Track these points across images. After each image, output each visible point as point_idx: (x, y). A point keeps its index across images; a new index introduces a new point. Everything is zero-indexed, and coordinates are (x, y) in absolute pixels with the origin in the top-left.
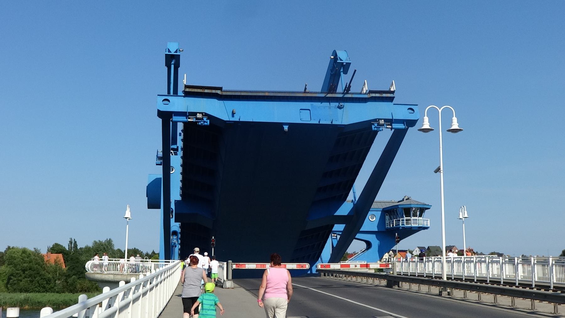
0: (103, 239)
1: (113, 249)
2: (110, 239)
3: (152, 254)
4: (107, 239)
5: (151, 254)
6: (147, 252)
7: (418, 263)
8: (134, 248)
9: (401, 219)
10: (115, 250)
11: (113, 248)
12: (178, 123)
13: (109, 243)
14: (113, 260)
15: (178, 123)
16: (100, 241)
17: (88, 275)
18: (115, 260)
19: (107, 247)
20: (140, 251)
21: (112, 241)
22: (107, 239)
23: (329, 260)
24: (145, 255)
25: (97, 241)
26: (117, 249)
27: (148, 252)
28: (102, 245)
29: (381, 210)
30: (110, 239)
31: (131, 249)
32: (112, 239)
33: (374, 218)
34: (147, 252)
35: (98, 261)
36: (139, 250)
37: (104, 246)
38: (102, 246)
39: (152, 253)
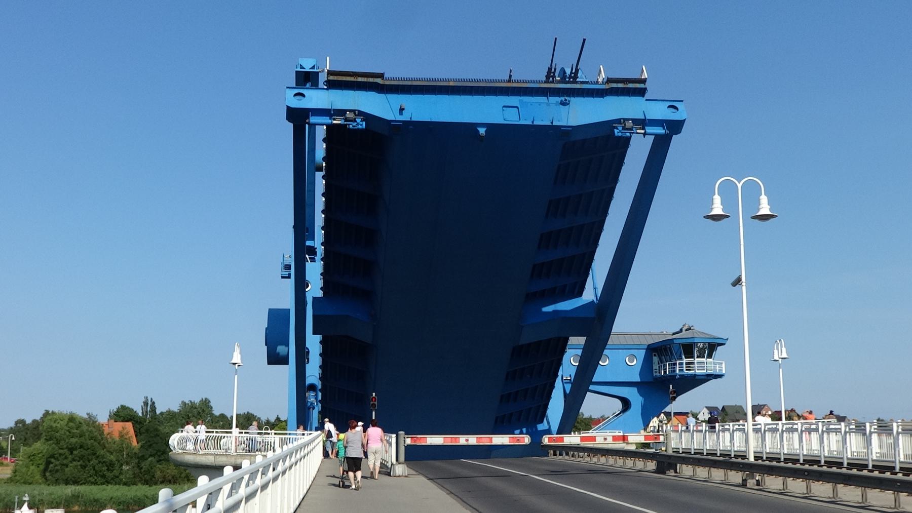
3: (275, 421)
4: (202, 399)
8: (246, 413)
19: (203, 411)
20: (256, 416)
28: (196, 408)
30: (206, 399)
37: (199, 409)
39: (276, 420)
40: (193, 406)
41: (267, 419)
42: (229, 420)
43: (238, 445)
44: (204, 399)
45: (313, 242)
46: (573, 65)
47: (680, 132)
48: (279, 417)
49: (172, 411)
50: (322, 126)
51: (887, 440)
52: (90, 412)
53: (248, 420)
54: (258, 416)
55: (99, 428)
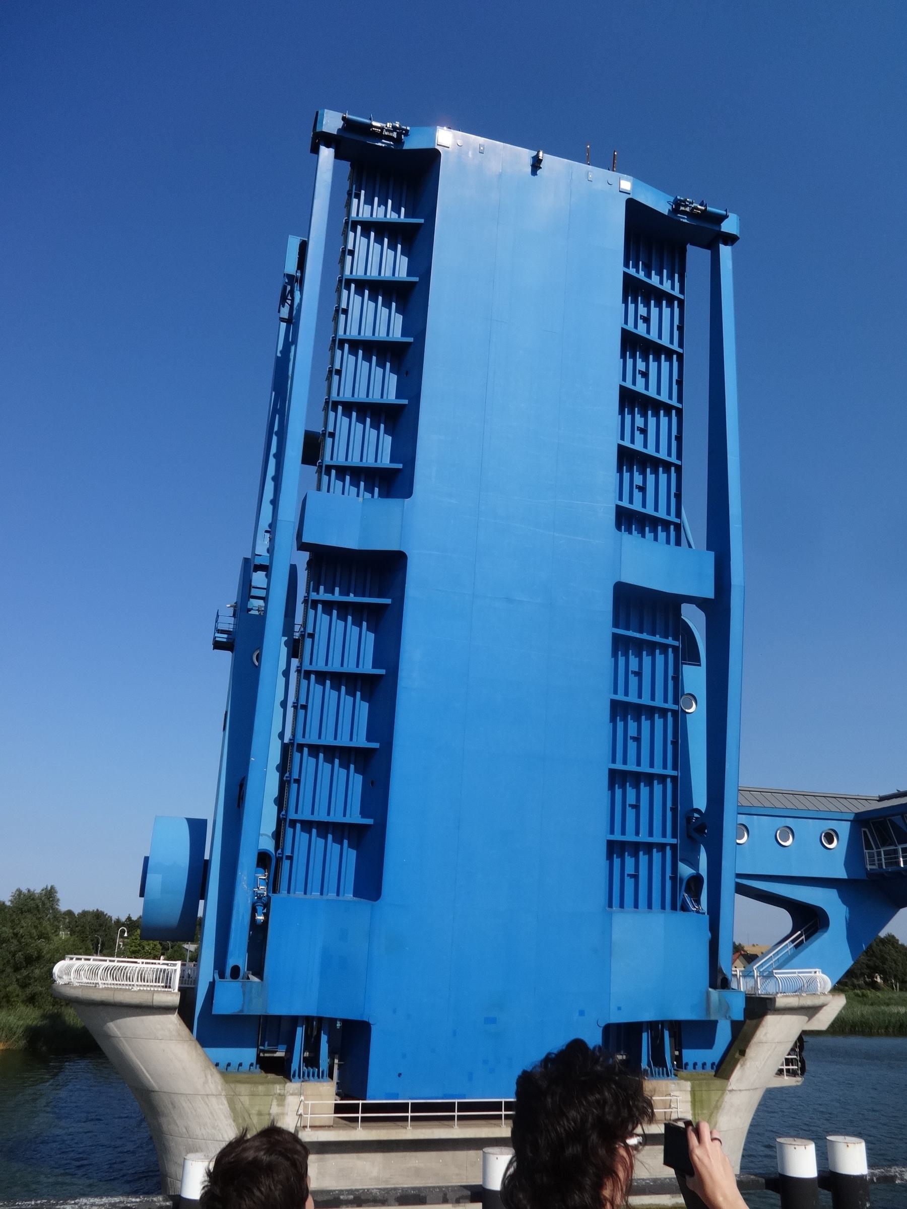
0: (38, 888)
1: (57, 909)
2: (52, 887)
3: (125, 921)
4: (47, 886)
5: (124, 921)
6: (118, 917)
7: (759, 979)
8: (95, 910)
9: (900, 848)
10: (59, 912)
11: (56, 906)
12: (370, 207)
13: (50, 895)
14: (106, 961)
15: (370, 207)
16: (29, 891)
17: (54, 987)
18: (118, 961)
19: (44, 904)
20: (106, 914)
21: (56, 892)
22: (47, 886)
23: (148, 875)
24: (114, 922)
25: (24, 891)
26: (66, 909)
27: (120, 917)
28: (33, 899)
29: (851, 817)
30: (52, 887)
31: (91, 910)
32: (57, 888)
33: (788, 839)
34: (118, 917)
35: (257, 1070)
36: (105, 913)
37: (38, 901)
38: (32, 902)
39: (127, 919)
40: (30, 896)
41: (117, 918)
42: (76, 917)
43: (763, 984)
44: (49, 888)
45: (317, 155)
46: (349, 495)
47: (274, 801)
48: (131, 916)
49: (84, 914)
50: (473, 1155)
51: (751, 982)
52: (304, 570)
53: (98, 918)
54: (109, 914)
55: (6, 1050)
